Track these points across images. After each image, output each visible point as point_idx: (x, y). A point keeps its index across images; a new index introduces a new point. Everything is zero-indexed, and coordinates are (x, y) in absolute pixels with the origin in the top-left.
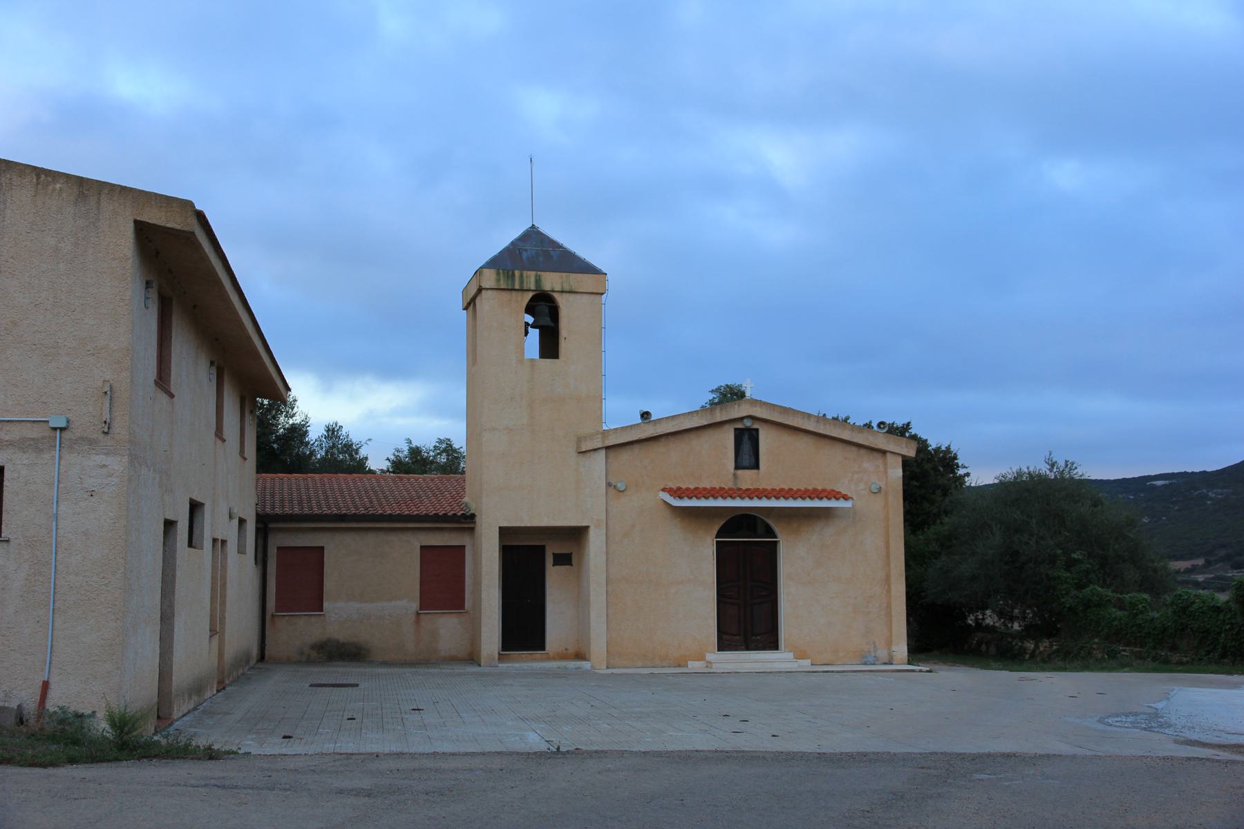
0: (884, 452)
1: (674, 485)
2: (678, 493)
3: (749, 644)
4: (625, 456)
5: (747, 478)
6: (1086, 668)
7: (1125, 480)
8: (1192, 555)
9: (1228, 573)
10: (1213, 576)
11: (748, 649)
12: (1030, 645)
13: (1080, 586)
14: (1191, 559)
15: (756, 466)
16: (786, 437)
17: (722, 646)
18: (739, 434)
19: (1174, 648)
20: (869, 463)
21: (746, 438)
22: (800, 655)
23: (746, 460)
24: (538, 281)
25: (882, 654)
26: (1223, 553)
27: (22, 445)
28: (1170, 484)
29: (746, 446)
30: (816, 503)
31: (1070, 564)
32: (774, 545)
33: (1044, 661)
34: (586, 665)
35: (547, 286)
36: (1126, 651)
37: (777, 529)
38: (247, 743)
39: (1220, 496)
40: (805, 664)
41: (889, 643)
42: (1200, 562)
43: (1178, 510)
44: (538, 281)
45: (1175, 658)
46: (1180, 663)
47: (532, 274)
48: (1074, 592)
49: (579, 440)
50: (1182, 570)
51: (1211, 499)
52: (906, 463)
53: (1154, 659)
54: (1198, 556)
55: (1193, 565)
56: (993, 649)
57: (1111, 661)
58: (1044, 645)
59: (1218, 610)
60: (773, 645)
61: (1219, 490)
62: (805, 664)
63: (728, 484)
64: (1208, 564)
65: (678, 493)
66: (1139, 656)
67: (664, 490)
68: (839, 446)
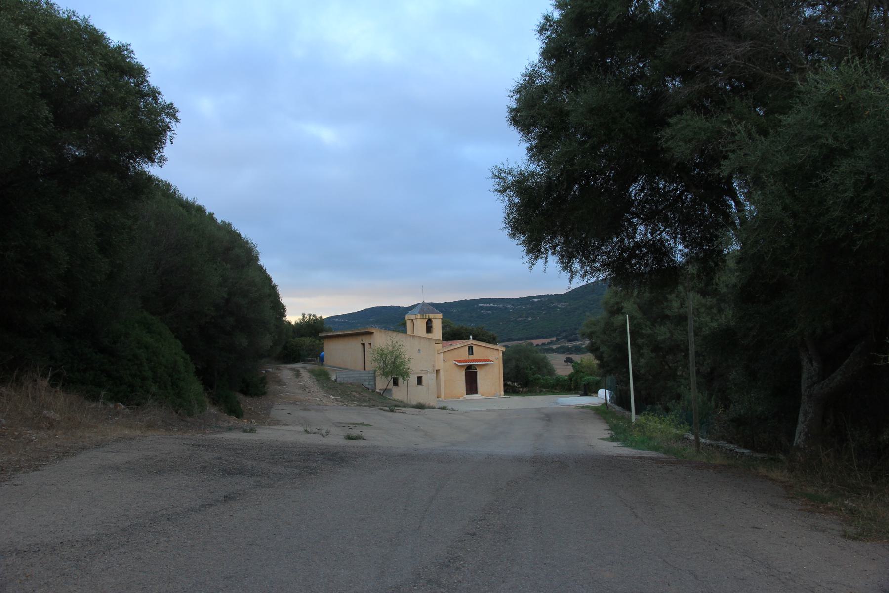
0: (498, 350)
1: (456, 360)
2: (458, 361)
3: (471, 394)
4: (446, 354)
5: (471, 357)
6: (537, 395)
7: (520, 299)
8: (551, 336)
9: (566, 344)
10: (559, 346)
11: (471, 394)
12: (521, 390)
13: (534, 375)
14: (550, 338)
15: (473, 354)
16: (478, 347)
17: (466, 394)
18: (469, 347)
19: (556, 389)
20: (495, 353)
21: (470, 348)
22: (482, 395)
23: (471, 353)
24: (429, 316)
25: (498, 394)
26: (564, 334)
27: (424, 373)
28: (541, 301)
29: (471, 350)
30: (485, 363)
31: (531, 369)
32: (476, 372)
33: (525, 393)
34: (440, 399)
35: (430, 317)
36: (544, 390)
37: (477, 368)
38: (44, 463)
39: (563, 307)
40: (483, 397)
41: (500, 392)
42: (554, 339)
43: (545, 314)
44: (429, 316)
45: (556, 391)
46: (557, 393)
47: (427, 315)
48: (532, 376)
49: (438, 351)
50: (546, 343)
51: (559, 308)
52: (503, 353)
53: (552, 392)
54: (553, 336)
55: (551, 341)
56: (511, 391)
57: (541, 393)
58: (525, 389)
59: (565, 380)
60: (476, 393)
61: (563, 304)
62: (483, 397)
63: (467, 359)
64: (558, 340)
65: (458, 361)
66: (548, 391)
67: (455, 361)
68: (489, 349)
